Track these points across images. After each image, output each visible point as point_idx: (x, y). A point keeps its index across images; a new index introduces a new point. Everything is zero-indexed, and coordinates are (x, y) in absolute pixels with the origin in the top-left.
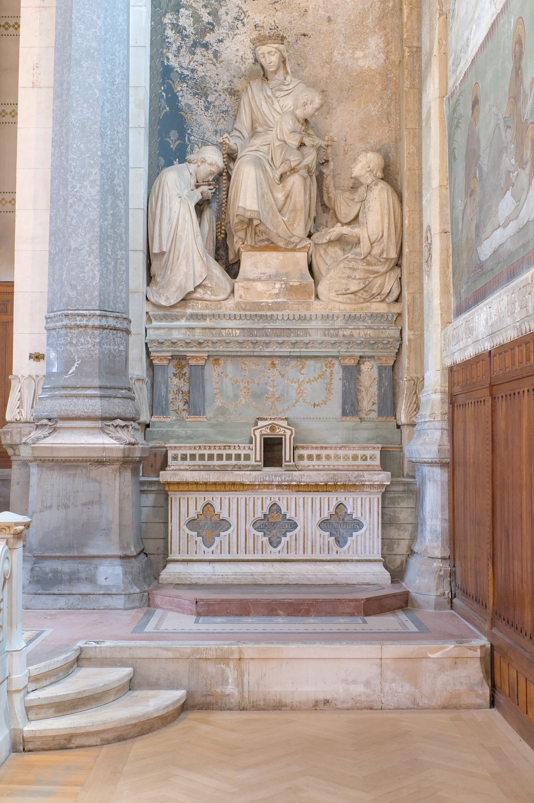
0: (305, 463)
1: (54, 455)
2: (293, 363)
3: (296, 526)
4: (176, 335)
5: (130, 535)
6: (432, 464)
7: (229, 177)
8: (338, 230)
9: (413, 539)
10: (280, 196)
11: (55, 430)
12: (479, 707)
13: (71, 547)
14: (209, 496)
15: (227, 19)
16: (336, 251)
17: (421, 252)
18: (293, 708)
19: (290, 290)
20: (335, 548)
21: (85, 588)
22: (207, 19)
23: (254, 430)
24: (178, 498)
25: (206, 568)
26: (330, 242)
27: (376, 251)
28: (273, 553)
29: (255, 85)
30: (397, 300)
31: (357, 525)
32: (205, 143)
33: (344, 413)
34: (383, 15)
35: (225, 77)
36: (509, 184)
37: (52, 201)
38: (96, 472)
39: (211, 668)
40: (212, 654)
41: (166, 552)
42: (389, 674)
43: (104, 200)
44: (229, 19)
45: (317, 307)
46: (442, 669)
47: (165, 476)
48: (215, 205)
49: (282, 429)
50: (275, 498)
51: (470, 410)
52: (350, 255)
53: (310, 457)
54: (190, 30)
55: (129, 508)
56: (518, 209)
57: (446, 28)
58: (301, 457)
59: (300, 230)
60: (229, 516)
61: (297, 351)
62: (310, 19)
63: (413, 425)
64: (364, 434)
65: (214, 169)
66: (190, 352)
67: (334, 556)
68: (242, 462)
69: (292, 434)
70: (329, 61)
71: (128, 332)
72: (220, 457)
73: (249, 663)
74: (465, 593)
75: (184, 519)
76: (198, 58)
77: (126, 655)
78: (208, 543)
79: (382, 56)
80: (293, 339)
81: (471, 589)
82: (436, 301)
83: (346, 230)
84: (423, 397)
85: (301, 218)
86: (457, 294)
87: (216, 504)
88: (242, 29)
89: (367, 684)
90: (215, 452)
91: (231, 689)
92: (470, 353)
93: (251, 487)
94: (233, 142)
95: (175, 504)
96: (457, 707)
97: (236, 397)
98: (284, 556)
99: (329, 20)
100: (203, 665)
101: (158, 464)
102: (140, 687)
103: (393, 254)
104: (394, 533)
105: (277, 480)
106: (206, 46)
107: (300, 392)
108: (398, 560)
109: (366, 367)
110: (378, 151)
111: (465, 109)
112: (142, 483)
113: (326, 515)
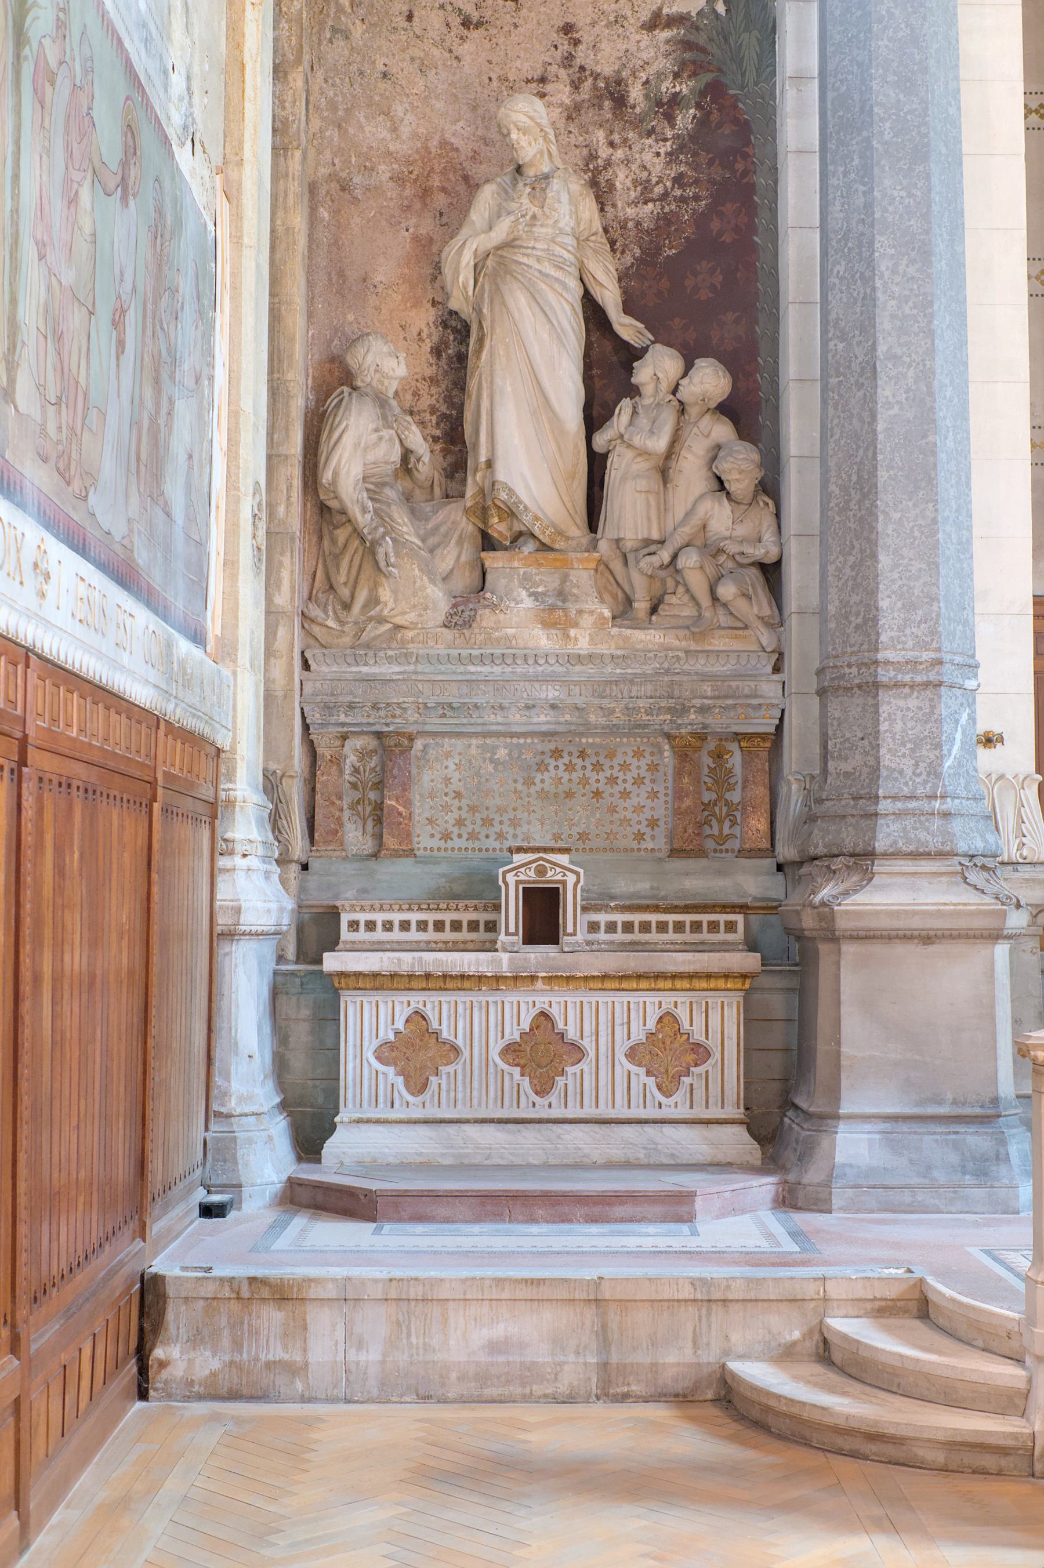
1: (928, 926)
3: (709, 1054)
14: (417, 999)
23: (505, 873)
24: (719, 1004)
49: (559, 870)
60: (707, 1038)
67: (652, 1113)
69: (578, 881)
73: (709, 1315)
78: (543, 1089)
98: (556, 1113)
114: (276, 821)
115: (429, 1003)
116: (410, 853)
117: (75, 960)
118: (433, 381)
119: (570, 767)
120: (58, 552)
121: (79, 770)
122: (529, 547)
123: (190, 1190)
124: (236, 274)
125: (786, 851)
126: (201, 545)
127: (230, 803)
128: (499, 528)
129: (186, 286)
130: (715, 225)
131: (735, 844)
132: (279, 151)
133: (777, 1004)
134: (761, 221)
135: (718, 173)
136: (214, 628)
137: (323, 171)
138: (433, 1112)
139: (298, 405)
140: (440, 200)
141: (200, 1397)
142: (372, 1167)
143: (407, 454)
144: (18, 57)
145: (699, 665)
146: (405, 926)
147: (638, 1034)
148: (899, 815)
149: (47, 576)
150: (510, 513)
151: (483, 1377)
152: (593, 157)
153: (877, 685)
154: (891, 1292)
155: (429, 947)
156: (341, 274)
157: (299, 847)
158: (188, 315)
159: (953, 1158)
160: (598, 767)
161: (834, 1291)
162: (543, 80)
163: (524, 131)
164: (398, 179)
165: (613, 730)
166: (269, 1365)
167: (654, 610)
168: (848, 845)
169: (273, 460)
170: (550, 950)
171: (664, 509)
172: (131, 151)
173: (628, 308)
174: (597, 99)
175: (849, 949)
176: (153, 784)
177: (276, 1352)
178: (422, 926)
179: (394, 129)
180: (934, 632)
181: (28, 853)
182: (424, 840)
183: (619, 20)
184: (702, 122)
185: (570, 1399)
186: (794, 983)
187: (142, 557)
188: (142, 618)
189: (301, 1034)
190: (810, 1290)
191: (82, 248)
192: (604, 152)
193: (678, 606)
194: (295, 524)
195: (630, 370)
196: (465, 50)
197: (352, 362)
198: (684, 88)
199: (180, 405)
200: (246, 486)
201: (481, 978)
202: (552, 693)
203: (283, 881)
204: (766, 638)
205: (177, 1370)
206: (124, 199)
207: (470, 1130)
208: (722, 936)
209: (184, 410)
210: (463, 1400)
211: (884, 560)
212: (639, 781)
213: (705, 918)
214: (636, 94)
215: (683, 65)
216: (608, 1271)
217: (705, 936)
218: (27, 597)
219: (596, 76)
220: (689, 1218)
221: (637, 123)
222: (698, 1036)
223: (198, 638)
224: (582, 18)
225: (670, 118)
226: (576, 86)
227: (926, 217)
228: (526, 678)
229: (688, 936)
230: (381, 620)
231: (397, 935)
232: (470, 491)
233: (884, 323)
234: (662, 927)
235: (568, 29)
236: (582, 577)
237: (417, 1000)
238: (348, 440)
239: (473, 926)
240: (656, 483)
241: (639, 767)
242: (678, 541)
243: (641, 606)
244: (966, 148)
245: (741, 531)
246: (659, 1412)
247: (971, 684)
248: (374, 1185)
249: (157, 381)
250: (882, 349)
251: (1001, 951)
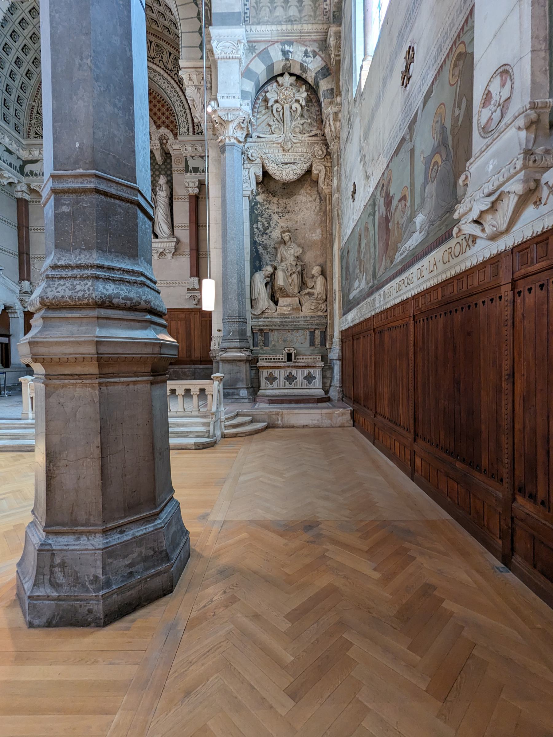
0: (299, 360)
2: (295, 331)
4: (260, 323)
5: (249, 382)
6: (336, 360)
7: (275, 275)
8: (308, 290)
9: (331, 382)
10: (290, 281)
11: (226, 352)
12: (350, 427)
13: (232, 386)
15: (273, 225)
16: (307, 297)
17: (333, 297)
18: (297, 427)
19: (293, 309)
20: (308, 385)
21: (237, 397)
22: (267, 225)
25: (271, 391)
26: (306, 294)
27: (319, 297)
28: (290, 386)
29: (282, 246)
30: (326, 311)
31: (315, 378)
32: (267, 265)
33: (310, 346)
34: (321, 223)
35: (273, 243)
36: (357, 277)
37: (223, 284)
38: (238, 364)
39: (274, 416)
40: (274, 413)
41: (259, 386)
42: (324, 418)
43: (238, 284)
44: (273, 225)
45: (302, 314)
46: (339, 416)
47: (258, 365)
48: (270, 284)
50: (291, 370)
51: (347, 343)
52: (311, 298)
53: (300, 359)
54: (262, 229)
55: (248, 374)
56: (360, 285)
57: (340, 227)
58: (298, 359)
59: (296, 291)
61: (296, 327)
62: (298, 224)
63: (331, 348)
64: (316, 352)
65: (270, 273)
66: (264, 328)
67: (308, 387)
68: (280, 360)
70: (304, 238)
71: (246, 323)
72: (274, 359)
74: (346, 396)
75: (264, 377)
76: (264, 238)
77: (250, 413)
78: (271, 384)
79: (321, 236)
80: (295, 324)
81: (348, 395)
82: (337, 312)
83: (310, 290)
84: (334, 340)
85: (297, 287)
86: (343, 309)
87: (273, 373)
88: (277, 228)
89: (318, 420)
90: (273, 358)
91: (280, 422)
92: (347, 327)
93: (283, 367)
94: (275, 264)
95: (261, 373)
96: (344, 427)
97: (278, 341)
99: (304, 224)
100: (272, 416)
101: (256, 361)
102: (255, 422)
103: (324, 298)
104: (325, 380)
105: (291, 365)
106: (267, 234)
107: (297, 340)
108: (327, 388)
109: (317, 332)
110: (320, 266)
111: (345, 254)
112: (251, 367)
113: (305, 375)
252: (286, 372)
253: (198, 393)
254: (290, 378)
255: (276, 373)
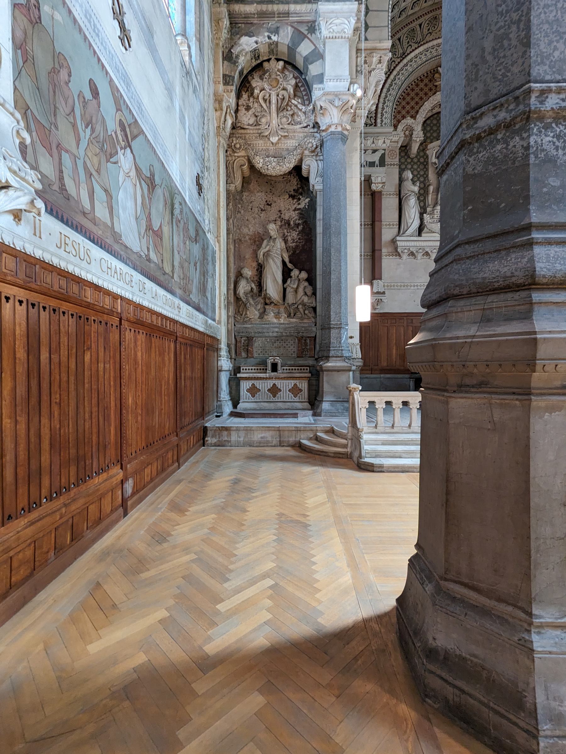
78: (274, 396)
98: (277, 400)
114: (229, 352)
115: (255, 382)
116: (253, 357)
117: (189, 373)
118: (257, 275)
119: (280, 343)
120: (182, 304)
121: (187, 341)
122: (273, 305)
123: (214, 413)
124: (220, 257)
125: (316, 357)
126: (214, 304)
127: (220, 349)
128: (268, 301)
129: (210, 259)
130: (306, 247)
131: (308, 356)
132: (228, 234)
133: (314, 382)
134: (313, 246)
135: (306, 237)
136: (217, 318)
137: (237, 238)
138: (255, 400)
139: (232, 280)
140: (257, 243)
141: (213, 446)
142: (246, 409)
143: (252, 288)
144: (172, 218)
145: (302, 325)
146: (252, 369)
147: (290, 387)
148: (334, 350)
149: (180, 309)
150: (269, 299)
151: (260, 443)
152: (284, 235)
153: (331, 328)
154: (328, 429)
155: (256, 373)
156: (240, 256)
157: (233, 356)
158: (210, 263)
159: (342, 408)
160: (285, 342)
161: (318, 429)
162: (275, 221)
163: (272, 230)
164: (250, 239)
165: (287, 336)
166: (225, 441)
167: (294, 315)
168: (325, 355)
169: (228, 290)
170: (276, 373)
171: (296, 298)
172: (197, 234)
173: (290, 262)
174: (285, 224)
175: (325, 373)
176: (204, 345)
177: (226, 439)
178: (255, 369)
179: (249, 230)
180: (340, 319)
181: (178, 355)
182: (255, 355)
183: (289, 209)
184: (303, 228)
185: (274, 446)
186: (316, 378)
187: (202, 306)
188: (201, 316)
189: (234, 387)
190: (314, 429)
191: (187, 252)
192: (286, 234)
193: (299, 315)
194: (232, 301)
195: (290, 273)
196: (262, 215)
197: (242, 272)
198: (300, 222)
199: (209, 280)
200: (222, 294)
201: (264, 378)
202: (277, 330)
203: (231, 362)
204: (313, 320)
205: (209, 442)
206: (196, 243)
207: (262, 403)
208: (305, 371)
209: (210, 281)
210: (256, 446)
211: (332, 306)
212: (292, 345)
213: (302, 368)
214: (292, 223)
215: (300, 217)
216: (281, 425)
217: (302, 371)
218: (176, 312)
219: (285, 220)
220: (297, 417)
221: (292, 228)
222: (300, 388)
223: (214, 320)
224: (282, 209)
225: (298, 227)
226: (281, 222)
227: (340, 245)
228: (272, 327)
229: (299, 371)
230: (247, 317)
231: (250, 371)
232: (263, 295)
233: (332, 264)
234: (295, 369)
235: (280, 211)
236: (282, 309)
237: (253, 382)
238: (241, 286)
239: (263, 369)
240: (294, 293)
241: (292, 342)
242: (298, 303)
243: (292, 315)
244: (348, 232)
245: (309, 301)
246: (289, 448)
247: (347, 328)
248: (244, 412)
249: (204, 276)
250: (332, 269)
251: (351, 373)
252: (270, 384)
253: (367, 407)
254: (274, 390)
255: (258, 384)
